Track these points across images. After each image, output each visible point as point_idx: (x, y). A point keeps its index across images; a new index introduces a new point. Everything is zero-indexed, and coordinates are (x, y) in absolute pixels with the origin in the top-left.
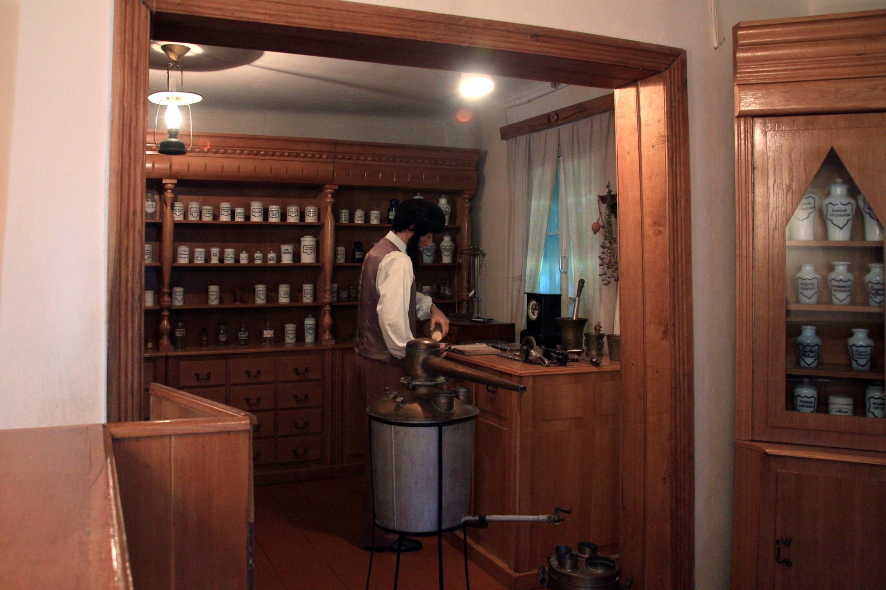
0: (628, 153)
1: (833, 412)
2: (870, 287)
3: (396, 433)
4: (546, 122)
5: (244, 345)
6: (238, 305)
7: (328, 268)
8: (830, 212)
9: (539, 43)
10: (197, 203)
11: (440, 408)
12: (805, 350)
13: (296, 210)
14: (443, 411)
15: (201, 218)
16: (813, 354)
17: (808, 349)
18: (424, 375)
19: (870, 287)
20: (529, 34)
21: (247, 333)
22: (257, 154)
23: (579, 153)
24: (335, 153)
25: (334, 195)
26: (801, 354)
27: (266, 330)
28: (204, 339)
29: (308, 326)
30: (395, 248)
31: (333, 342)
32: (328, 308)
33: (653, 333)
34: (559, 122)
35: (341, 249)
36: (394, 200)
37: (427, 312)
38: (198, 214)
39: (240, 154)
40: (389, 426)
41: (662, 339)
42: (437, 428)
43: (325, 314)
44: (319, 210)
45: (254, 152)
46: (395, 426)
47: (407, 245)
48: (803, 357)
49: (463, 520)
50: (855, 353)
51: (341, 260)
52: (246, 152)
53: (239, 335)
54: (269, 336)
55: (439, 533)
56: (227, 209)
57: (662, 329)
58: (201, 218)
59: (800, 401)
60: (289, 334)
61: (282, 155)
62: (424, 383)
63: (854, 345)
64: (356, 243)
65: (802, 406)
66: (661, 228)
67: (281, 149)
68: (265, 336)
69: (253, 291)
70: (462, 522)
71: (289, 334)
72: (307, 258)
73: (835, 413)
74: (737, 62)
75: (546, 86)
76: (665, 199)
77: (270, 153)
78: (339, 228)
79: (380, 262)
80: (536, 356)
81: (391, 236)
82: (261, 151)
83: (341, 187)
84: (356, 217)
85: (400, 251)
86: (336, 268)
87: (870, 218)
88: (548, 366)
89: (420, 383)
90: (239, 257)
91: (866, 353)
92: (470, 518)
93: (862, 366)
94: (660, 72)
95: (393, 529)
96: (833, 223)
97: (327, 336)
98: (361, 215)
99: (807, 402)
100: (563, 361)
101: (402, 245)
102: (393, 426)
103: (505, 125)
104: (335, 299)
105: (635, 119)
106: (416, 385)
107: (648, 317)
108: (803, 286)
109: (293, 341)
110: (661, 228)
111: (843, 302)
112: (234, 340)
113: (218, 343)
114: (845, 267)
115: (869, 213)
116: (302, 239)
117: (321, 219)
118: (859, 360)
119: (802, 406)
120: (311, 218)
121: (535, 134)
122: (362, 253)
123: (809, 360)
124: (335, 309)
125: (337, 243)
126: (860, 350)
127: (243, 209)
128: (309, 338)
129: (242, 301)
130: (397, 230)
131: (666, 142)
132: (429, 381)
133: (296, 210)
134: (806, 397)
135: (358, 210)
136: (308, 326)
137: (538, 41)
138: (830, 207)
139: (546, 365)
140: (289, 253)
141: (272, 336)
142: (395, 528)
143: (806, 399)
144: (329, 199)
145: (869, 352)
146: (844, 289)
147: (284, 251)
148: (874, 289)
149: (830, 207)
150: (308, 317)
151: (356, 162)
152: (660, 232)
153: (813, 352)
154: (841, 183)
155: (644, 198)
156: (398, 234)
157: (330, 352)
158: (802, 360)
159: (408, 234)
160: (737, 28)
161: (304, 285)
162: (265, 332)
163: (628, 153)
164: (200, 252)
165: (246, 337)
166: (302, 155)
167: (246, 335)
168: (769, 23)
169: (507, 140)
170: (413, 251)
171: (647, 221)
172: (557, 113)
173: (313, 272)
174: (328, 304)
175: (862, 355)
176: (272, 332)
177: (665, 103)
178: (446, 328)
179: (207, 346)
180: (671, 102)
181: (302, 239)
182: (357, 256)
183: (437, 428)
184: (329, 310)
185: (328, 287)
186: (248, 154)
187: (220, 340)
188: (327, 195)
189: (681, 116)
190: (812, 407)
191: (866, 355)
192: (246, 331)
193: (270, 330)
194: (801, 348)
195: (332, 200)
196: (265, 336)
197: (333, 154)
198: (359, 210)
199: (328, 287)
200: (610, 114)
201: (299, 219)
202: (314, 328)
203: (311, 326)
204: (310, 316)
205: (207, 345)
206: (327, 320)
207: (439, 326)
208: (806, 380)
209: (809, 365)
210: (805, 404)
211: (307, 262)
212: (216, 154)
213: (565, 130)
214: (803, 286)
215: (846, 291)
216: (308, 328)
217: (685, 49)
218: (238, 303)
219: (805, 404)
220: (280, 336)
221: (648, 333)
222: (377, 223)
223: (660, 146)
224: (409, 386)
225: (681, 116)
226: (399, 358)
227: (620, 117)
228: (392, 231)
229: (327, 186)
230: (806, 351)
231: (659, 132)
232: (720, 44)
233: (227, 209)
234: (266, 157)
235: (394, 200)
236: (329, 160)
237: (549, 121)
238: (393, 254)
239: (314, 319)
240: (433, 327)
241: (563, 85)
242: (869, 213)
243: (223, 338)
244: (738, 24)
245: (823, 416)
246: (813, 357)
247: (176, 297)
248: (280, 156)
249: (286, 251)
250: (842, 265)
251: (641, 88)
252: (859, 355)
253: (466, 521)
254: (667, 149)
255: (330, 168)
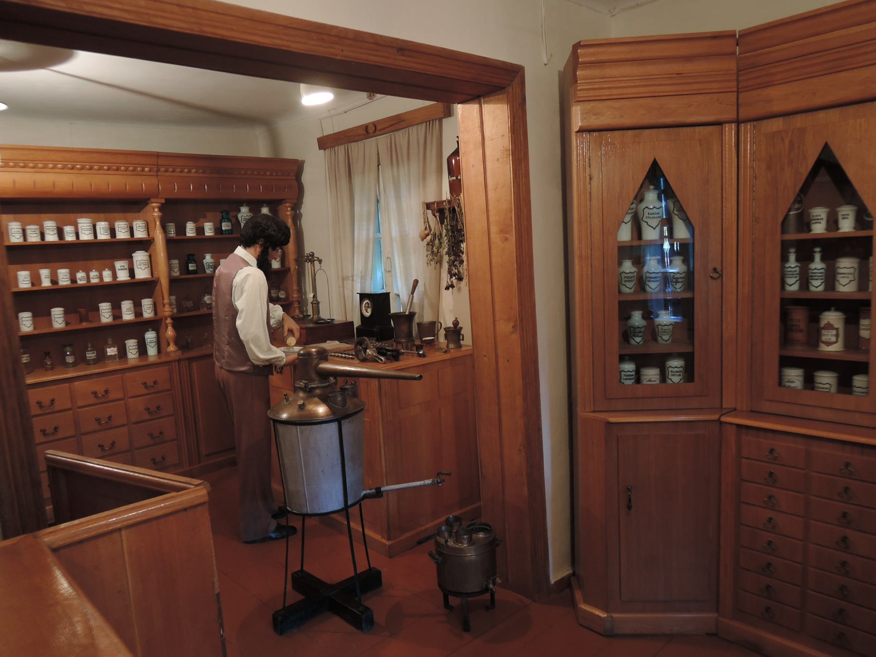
0: (473, 166)
1: (645, 382)
2: (672, 276)
3: (302, 432)
4: (364, 132)
5: (94, 364)
6: (85, 325)
7: (164, 282)
8: (646, 215)
9: (404, 58)
10: (18, 223)
11: (337, 406)
12: (635, 331)
13: (126, 226)
14: (340, 408)
15: (25, 239)
16: (641, 334)
17: (638, 330)
18: (317, 379)
19: (672, 276)
20: (395, 47)
21: (95, 352)
22: (72, 168)
23: (398, 164)
24: (158, 165)
25: (161, 209)
26: (632, 335)
27: (110, 348)
28: (49, 363)
29: (149, 340)
30: (247, 264)
31: (179, 353)
32: (169, 321)
33: (504, 327)
34: (377, 133)
35: (175, 262)
36: (224, 211)
37: (279, 320)
38: (21, 235)
39: (53, 168)
40: (295, 427)
41: (512, 333)
42: (337, 423)
43: (167, 327)
44: (147, 223)
45: (69, 166)
46: (300, 427)
47: (257, 260)
48: (633, 337)
49: (363, 494)
50: (660, 331)
51: (176, 273)
52: (59, 166)
53: (87, 355)
54: (113, 354)
55: (345, 510)
56: (52, 228)
57: (512, 324)
58: (25, 239)
59: (624, 375)
60: (131, 349)
61: (100, 169)
62: (319, 385)
63: (660, 324)
64: (188, 255)
65: (626, 379)
66: (507, 236)
67: (99, 163)
68: (109, 354)
69: (97, 309)
70: (361, 496)
71: (131, 349)
72: (142, 274)
73: (646, 383)
74: (578, 79)
75: (362, 96)
76: (511, 209)
77: (88, 167)
78: (169, 242)
79: (234, 278)
80: (372, 355)
81: (240, 251)
82: (78, 165)
83: (166, 200)
84: (188, 230)
85: (251, 266)
86: (173, 281)
87: (678, 219)
88: (385, 363)
89: (315, 386)
90: (75, 276)
91: (668, 331)
92: (368, 491)
93: (666, 341)
94: (504, 88)
95: (306, 513)
96: (648, 225)
97: (172, 348)
98: (193, 228)
99: (630, 375)
100: (395, 356)
101: (253, 261)
102: (298, 427)
103: (322, 136)
104: (175, 311)
105: (479, 134)
106: (311, 388)
107: (498, 314)
108: (626, 279)
109: (137, 356)
110: (507, 236)
111: (655, 290)
112: (80, 360)
113: (65, 364)
114: (656, 261)
115: (677, 215)
116: (133, 255)
117: (151, 233)
118: (662, 336)
119: (626, 379)
120: (140, 234)
121: (353, 144)
122: (195, 264)
123: (638, 339)
124: (179, 322)
125: (170, 256)
126: (664, 329)
127: (73, 227)
128: (152, 351)
129: (87, 320)
130: (247, 245)
131: (511, 156)
132: (322, 383)
133: (126, 226)
134: (629, 371)
135: (188, 222)
136: (149, 340)
137: (403, 55)
138: (646, 211)
139: (383, 362)
140: (125, 269)
141: (116, 353)
142: (308, 512)
143: (629, 373)
144: (156, 213)
145: (671, 329)
146: (656, 279)
147: (120, 268)
148: (675, 278)
149: (646, 211)
150: (148, 331)
151: (187, 175)
152: (506, 239)
153: (641, 332)
154: (654, 189)
155: (490, 208)
156: (247, 249)
157: (177, 363)
158: (633, 340)
159: (258, 249)
160: (577, 46)
161: (142, 301)
162: (108, 350)
163: (473, 166)
164: (45, 273)
165: (94, 356)
166: (139, 168)
167: (95, 354)
168: (604, 42)
169: (325, 150)
170: (263, 264)
171: (494, 229)
172: (375, 124)
173: (146, 288)
174: (169, 317)
175: (666, 332)
176: (115, 349)
177: (509, 119)
178: (297, 334)
179: (52, 370)
180: (514, 118)
181: (133, 255)
182: (191, 268)
183: (337, 423)
184: (171, 323)
185: (166, 301)
186: (63, 169)
187: (67, 361)
188: (154, 208)
189: (521, 131)
190: (633, 379)
191: (669, 332)
192: (93, 351)
193: (114, 347)
194: (632, 329)
195: (160, 214)
196: (109, 354)
197: (156, 166)
198: (190, 222)
199: (166, 301)
200: (426, 125)
201: (129, 234)
202: (155, 341)
203: (152, 339)
204: (150, 329)
205: (52, 369)
206: (170, 332)
207: (291, 331)
208: (627, 358)
209: (638, 343)
210: (628, 377)
211: (142, 277)
212: (24, 169)
213: (382, 141)
214: (626, 279)
215: (657, 281)
216: (149, 341)
217: (523, 66)
218: (84, 323)
219: (628, 377)
220: (122, 353)
221: (498, 328)
222: (212, 234)
223: (505, 159)
224: (306, 389)
225: (521, 131)
226: (261, 366)
227: (463, 132)
228: (240, 246)
229: (152, 200)
230: (636, 332)
231: (503, 147)
232: (549, 60)
233: (52, 228)
234: (83, 171)
235: (224, 211)
236: (152, 173)
237: (368, 131)
238: (246, 270)
239: (155, 332)
240: (286, 333)
241: (378, 96)
242: (677, 215)
243: (70, 359)
244: (580, 42)
245: (664, 384)
246: (641, 336)
247: (24, 323)
248: (99, 170)
249: (122, 268)
250: (654, 259)
251: (486, 105)
252: (664, 332)
253: (364, 495)
254: (511, 162)
255: (154, 181)
